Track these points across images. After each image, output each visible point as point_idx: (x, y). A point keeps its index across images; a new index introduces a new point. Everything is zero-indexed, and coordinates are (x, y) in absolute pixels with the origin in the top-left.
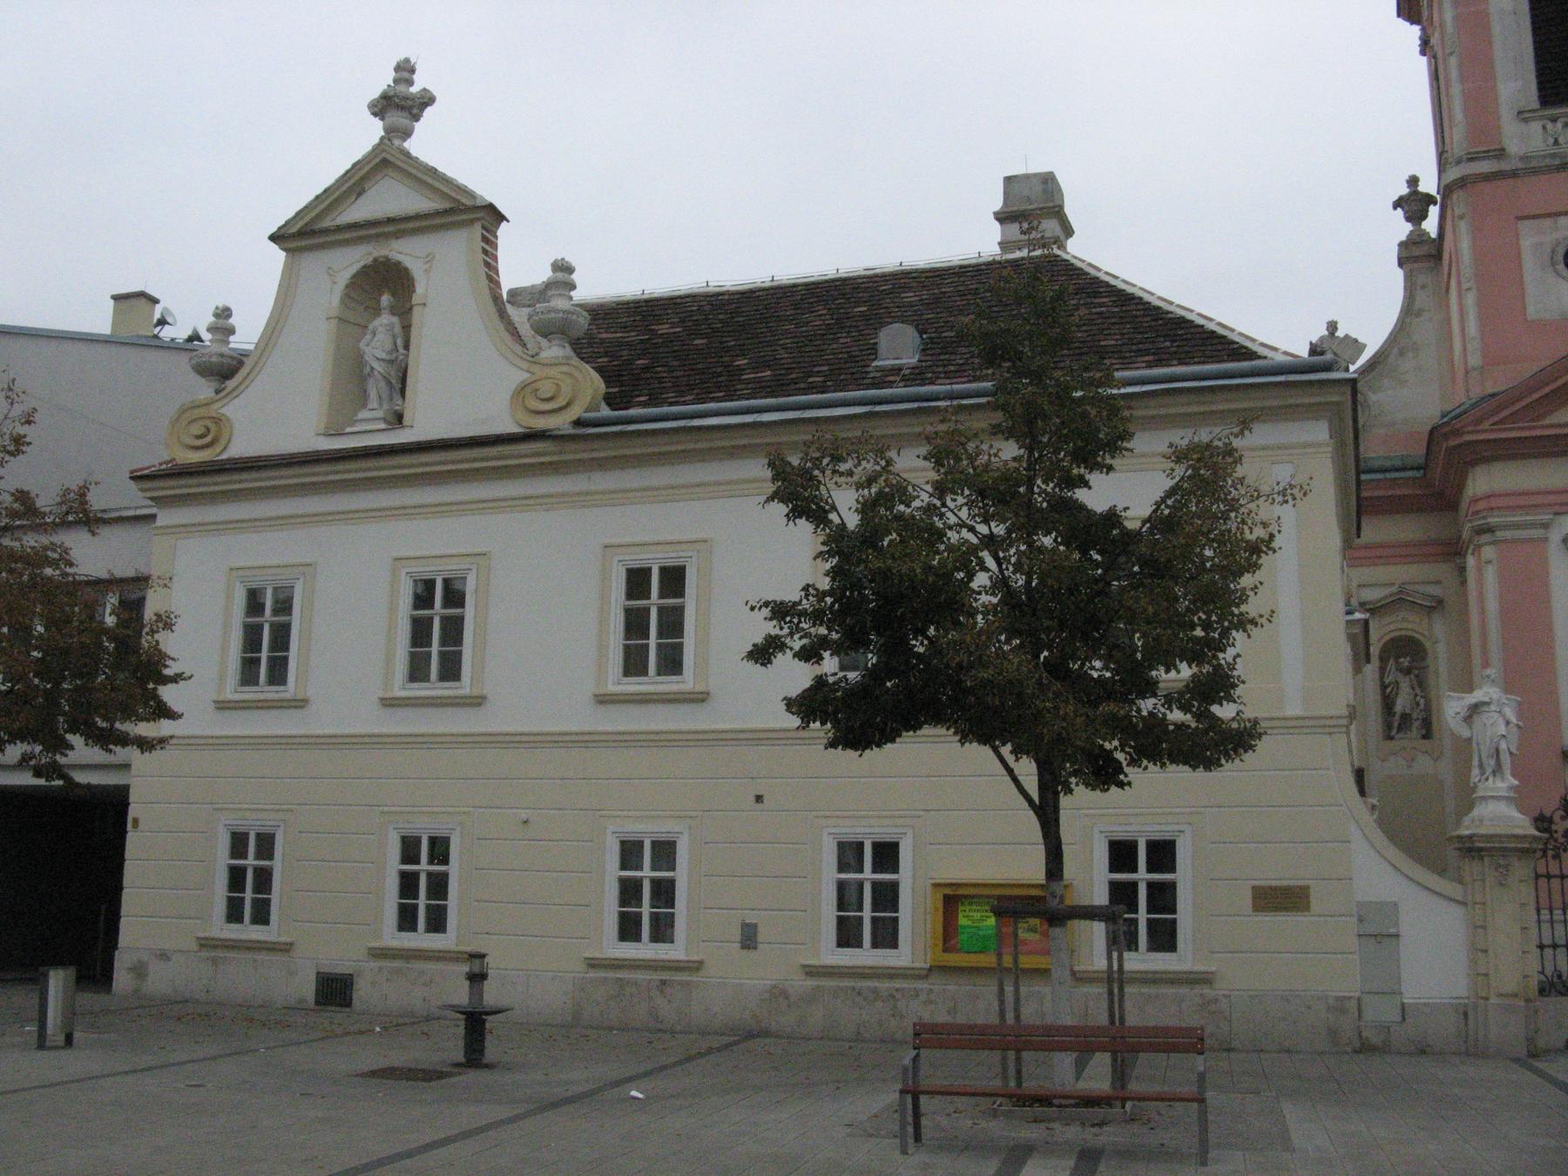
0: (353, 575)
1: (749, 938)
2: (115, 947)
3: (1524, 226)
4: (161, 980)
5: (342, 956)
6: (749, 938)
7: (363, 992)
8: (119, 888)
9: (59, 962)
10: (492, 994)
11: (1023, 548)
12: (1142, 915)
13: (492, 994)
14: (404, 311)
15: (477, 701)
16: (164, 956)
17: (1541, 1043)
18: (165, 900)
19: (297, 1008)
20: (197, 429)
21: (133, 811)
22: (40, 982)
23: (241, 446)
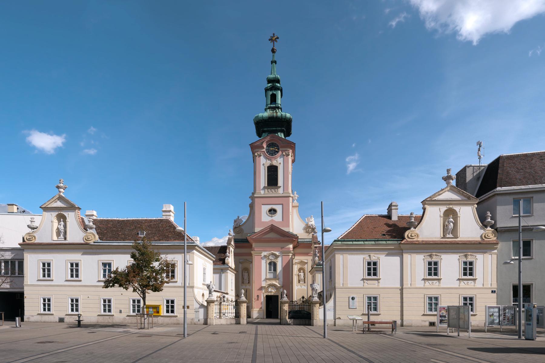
0: (60, 262)
1: (121, 312)
2: (24, 315)
3: (263, 206)
4: (32, 319)
5: (62, 316)
6: (121, 312)
7: (66, 320)
8: (24, 307)
9: (18, 316)
10: (81, 319)
11: (164, 275)
12: (170, 274)
13: (81, 319)
14: (65, 222)
15: (80, 281)
16: (32, 316)
17: (377, 282)
18: (32, 307)
19: (56, 322)
20: (30, 237)
21: (25, 296)
22: (15, 320)
23: (37, 241)
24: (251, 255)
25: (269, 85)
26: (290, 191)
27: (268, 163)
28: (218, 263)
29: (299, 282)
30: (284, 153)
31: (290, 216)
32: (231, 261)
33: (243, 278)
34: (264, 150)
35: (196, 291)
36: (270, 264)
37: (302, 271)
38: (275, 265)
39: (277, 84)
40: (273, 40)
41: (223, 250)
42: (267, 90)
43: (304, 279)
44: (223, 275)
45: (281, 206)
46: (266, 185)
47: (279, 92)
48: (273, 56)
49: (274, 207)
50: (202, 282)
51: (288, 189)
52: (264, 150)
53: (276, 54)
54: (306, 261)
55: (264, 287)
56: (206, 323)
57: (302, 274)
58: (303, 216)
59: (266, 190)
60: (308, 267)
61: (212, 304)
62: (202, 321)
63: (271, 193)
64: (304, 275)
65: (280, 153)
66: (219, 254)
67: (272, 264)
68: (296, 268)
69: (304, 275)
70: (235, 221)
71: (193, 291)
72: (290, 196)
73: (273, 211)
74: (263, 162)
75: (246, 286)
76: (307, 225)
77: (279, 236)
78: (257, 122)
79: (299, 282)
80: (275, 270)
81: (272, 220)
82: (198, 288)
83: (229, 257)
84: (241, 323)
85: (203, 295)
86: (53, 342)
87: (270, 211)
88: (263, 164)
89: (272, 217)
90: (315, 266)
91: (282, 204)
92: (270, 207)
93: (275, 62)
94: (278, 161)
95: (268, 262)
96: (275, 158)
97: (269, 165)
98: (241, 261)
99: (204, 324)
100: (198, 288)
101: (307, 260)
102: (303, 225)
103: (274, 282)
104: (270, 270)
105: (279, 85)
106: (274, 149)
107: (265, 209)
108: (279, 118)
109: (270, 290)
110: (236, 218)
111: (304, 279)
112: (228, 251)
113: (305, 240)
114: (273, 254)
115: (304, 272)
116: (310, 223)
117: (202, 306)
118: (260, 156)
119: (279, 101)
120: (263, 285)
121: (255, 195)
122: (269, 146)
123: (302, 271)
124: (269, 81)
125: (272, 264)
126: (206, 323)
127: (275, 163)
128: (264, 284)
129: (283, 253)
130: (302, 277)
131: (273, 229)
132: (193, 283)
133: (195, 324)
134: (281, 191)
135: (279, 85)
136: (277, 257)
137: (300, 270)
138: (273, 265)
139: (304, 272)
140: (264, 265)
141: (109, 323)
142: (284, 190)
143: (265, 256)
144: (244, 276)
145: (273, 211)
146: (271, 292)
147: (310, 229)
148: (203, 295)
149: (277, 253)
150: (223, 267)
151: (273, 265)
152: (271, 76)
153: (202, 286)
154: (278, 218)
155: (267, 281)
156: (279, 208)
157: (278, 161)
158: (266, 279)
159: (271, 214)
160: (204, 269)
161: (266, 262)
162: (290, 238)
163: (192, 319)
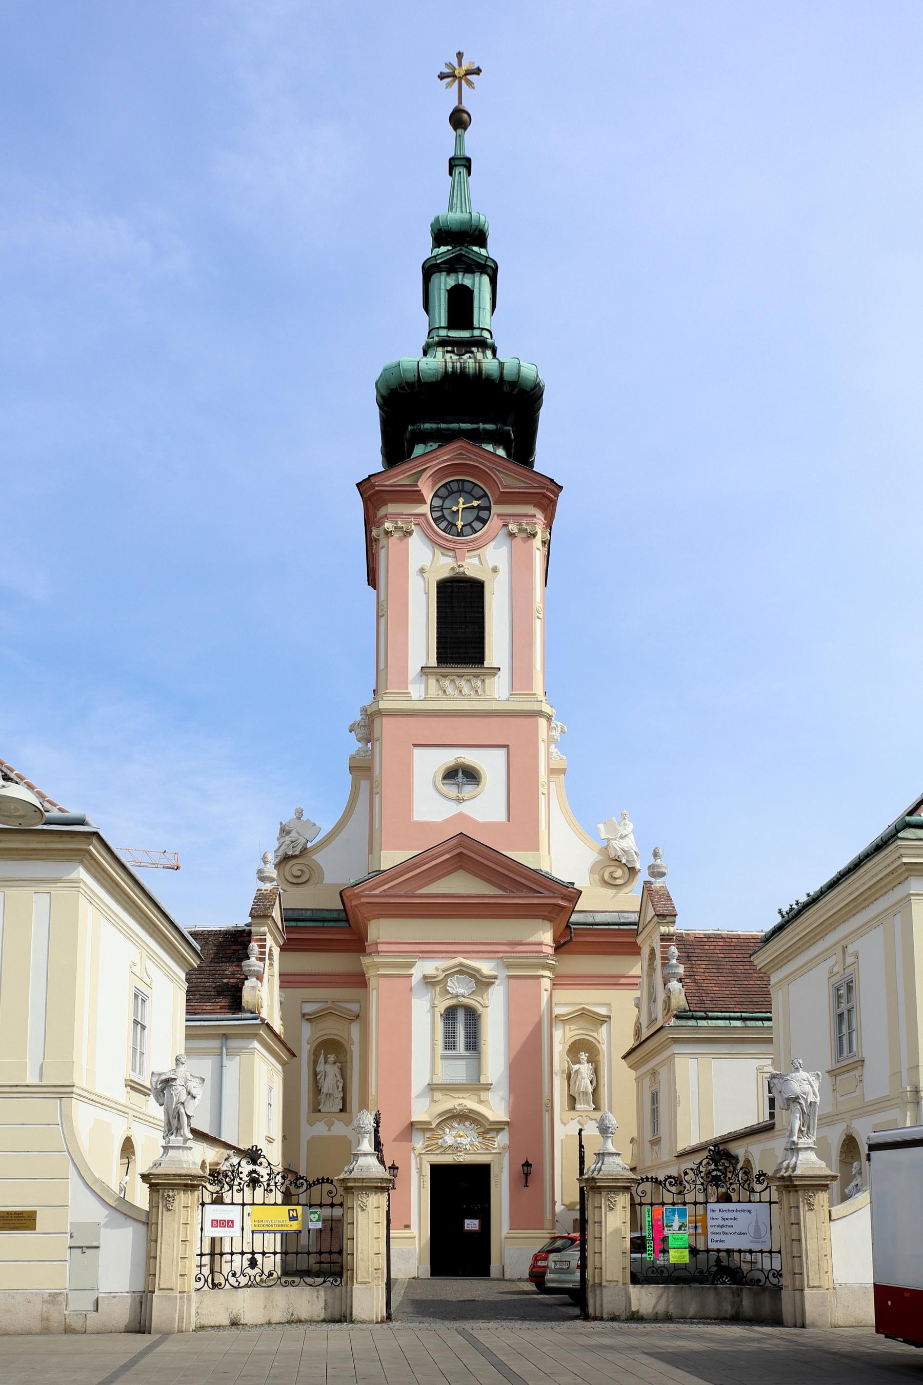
3: (417, 752)
24: (359, 981)
25: (443, 249)
26: (539, 689)
27: (444, 566)
28: (208, 1006)
29: (572, 1107)
30: (513, 527)
31: (543, 800)
32: (265, 993)
33: (317, 1089)
34: (425, 509)
35: (83, 1116)
36: (450, 1014)
37: (584, 1056)
38: (473, 1017)
39: (475, 249)
40: (458, 75)
41: (232, 946)
42: (429, 271)
43: (595, 1091)
44: (232, 1066)
45: (502, 753)
46: (433, 662)
47: (486, 279)
48: (459, 140)
49: (470, 757)
50: (126, 1072)
51: (529, 683)
52: (425, 509)
53: (469, 134)
54: (603, 1011)
55: (424, 1127)
56: (140, 1325)
57: (585, 1069)
58: (582, 815)
59: (432, 681)
60: (616, 1038)
61: (182, 1198)
62: (120, 1312)
63: (458, 692)
64: (596, 1071)
65: (494, 523)
66: (217, 971)
67: (461, 1016)
68: (561, 1039)
69: (596, 1071)
70: (284, 831)
71: (66, 1120)
72: (539, 714)
73: (462, 775)
74: (422, 562)
75: (330, 1125)
76: (605, 850)
77: (497, 885)
78: (440, 230)
79: (572, 1107)
80: (473, 1044)
81: (461, 816)
82: (95, 1101)
83: (260, 978)
84: (357, 1313)
85: (128, 1148)
86: (581, 1146)
87: (451, 774)
88: (422, 571)
89: (459, 800)
90: (673, 1022)
91: (507, 746)
92: (449, 757)
93: (467, 163)
94: (490, 560)
95: (443, 1004)
96: (475, 547)
97: (445, 574)
98: (309, 1008)
99: (128, 1331)
100: (95, 1101)
101: (608, 1005)
102: (591, 856)
103: (470, 1103)
104: (450, 1044)
105: (483, 252)
106: (466, 508)
107: (428, 764)
108: (489, 380)
109: (449, 1140)
110: (288, 816)
111: (595, 1091)
112: (254, 946)
113: (599, 918)
114: (463, 971)
115: (593, 1060)
116: (619, 845)
117: (122, 1209)
118: (409, 533)
119: (482, 316)
120: (414, 1118)
121: (383, 705)
122: (447, 492)
123: (584, 1056)
124: (441, 235)
125: (461, 1016)
126: (140, 1325)
127: (471, 567)
128: (421, 1111)
129: (509, 966)
130: (585, 1083)
131: (466, 853)
132: (69, 1066)
133: (68, 1330)
134: (498, 690)
135: (483, 252)
136: (483, 983)
137: (576, 1049)
138: (462, 1024)
139: (593, 1060)
140: (424, 1018)
141: (611, 1173)
142: (512, 687)
143: (429, 981)
144: (326, 1070)
145: (462, 775)
146: (456, 1148)
147: (616, 868)
148: (128, 1148)
149: (486, 967)
150: (229, 1021)
151: (462, 1024)
152: (455, 217)
153: (122, 1095)
154: (485, 808)
155: (438, 1095)
156: (492, 765)
157: (490, 560)
158: (433, 1088)
159: (452, 790)
160: (139, 998)
161: (433, 1007)
162: (548, 899)
163: (54, 1298)
